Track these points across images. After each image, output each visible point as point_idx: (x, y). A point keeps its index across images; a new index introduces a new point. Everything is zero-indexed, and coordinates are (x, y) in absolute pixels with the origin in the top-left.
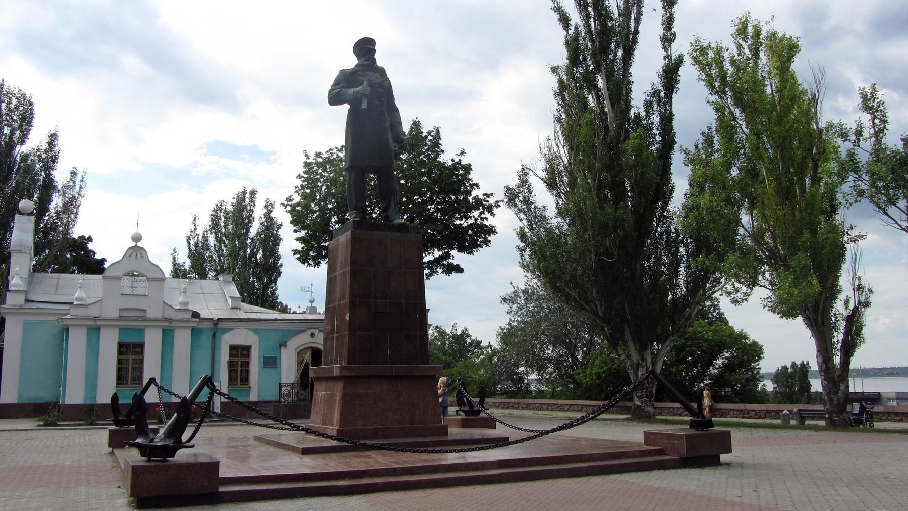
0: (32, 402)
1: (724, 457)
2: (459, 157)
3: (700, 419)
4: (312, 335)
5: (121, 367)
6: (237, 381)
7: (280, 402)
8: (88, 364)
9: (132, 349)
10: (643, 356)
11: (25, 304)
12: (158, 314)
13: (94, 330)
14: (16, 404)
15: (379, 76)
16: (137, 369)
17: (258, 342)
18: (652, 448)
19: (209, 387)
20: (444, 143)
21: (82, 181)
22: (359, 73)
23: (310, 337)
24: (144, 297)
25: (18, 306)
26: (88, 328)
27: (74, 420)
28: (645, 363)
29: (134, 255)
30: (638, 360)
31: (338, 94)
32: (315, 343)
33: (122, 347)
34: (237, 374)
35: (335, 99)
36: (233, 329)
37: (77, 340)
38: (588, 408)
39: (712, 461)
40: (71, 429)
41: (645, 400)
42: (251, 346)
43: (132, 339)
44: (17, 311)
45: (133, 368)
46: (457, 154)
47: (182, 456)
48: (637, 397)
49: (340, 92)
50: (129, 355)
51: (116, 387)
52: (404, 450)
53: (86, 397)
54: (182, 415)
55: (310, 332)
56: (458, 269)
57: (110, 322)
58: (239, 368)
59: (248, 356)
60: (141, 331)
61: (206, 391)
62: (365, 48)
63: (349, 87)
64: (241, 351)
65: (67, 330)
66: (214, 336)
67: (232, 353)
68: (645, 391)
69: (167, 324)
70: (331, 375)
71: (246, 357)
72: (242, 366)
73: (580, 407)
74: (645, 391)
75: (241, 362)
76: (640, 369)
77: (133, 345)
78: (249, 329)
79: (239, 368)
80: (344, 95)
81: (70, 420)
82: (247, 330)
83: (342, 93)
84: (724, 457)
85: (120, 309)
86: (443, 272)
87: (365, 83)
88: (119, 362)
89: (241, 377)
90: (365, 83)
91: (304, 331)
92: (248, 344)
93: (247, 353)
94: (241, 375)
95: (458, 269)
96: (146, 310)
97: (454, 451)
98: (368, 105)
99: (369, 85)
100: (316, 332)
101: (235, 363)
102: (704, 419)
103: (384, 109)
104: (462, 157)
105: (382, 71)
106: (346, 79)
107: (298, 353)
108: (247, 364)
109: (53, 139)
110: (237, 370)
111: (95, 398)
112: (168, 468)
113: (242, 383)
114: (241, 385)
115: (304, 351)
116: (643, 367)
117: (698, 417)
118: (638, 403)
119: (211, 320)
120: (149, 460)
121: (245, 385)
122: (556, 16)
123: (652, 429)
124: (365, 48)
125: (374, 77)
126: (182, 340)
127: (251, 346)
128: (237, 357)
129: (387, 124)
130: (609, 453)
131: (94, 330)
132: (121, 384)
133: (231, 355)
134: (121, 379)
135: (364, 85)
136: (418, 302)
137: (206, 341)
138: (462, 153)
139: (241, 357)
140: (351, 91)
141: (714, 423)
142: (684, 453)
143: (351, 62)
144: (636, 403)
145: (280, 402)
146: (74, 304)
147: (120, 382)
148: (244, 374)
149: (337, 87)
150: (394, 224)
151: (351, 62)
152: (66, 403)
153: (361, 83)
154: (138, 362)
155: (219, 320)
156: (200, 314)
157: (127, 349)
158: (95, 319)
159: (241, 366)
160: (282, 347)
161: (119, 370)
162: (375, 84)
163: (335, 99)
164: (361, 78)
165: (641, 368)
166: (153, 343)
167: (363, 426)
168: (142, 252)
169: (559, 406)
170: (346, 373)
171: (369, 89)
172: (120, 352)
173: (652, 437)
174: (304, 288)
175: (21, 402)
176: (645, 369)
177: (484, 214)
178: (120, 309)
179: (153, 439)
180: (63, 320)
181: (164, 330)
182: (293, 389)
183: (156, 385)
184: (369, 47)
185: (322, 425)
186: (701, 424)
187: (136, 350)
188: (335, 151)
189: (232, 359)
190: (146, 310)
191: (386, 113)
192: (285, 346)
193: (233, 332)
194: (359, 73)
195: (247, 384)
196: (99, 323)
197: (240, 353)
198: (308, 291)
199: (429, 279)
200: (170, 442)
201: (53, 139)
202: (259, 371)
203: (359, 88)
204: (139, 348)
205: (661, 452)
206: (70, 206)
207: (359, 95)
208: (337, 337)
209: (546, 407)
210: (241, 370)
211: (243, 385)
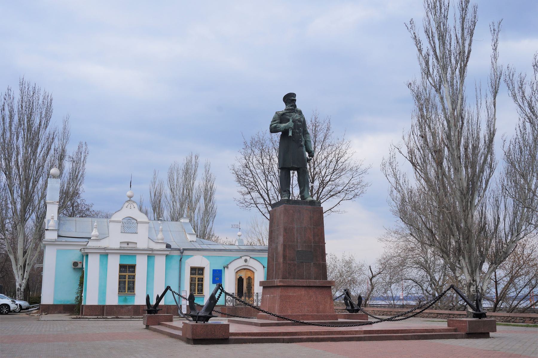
0: (62, 303)
1: (491, 334)
3: (478, 312)
4: (246, 261)
6: (195, 291)
7: (225, 306)
10: (473, 278)
11: (58, 238)
12: (145, 246)
14: (52, 305)
15: (298, 115)
16: (131, 282)
17: (209, 265)
18: (451, 328)
19: (220, 289)
22: (287, 114)
23: (244, 261)
25: (54, 239)
26: (100, 255)
27: (92, 315)
28: (475, 283)
29: (129, 206)
30: (470, 280)
31: (275, 127)
32: (247, 266)
34: (195, 287)
35: (273, 130)
36: (193, 256)
38: (441, 316)
39: (485, 335)
40: (102, 321)
42: (204, 267)
44: (52, 243)
47: (211, 321)
53: (99, 300)
54: (212, 302)
55: (244, 258)
58: (197, 283)
60: (134, 256)
62: (290, 99)
63: (281, 123)
64: (198, 271)
65: (87, 256)
66: (181, 260)
67: (121, 269)
69: (150, 252)
70: (273, 285)
71: (132, 273)
72: (198, 281)
73: (436, 314)
75: (198, 278)
76: (472, 287)
77: (134, 281)
78: (203, 256)
79: (197, 283)
81: (90, 315)
82: (202, 256)
83: (277, 126)
84: (491, 334)
85: (120, 242)
87: (291, 120)
88: (120, 277)
89: (198, 289)
90: (291, 120)
91: (241, 257)
92: (202, 266)
94: (198, 287)
96: (137, 243)
98: (292, 134)
99: (293, 121)
100: (248, 258)
101: (194, 279)
102: (480, 313)
103: (301, 134)
105: (300, 113)
106: (281, 118)
107: (236, 273)
108: (201, 280)
110: (195, 284)
111: (105, 301)
112: (207, 325)
113: (199, 293)
115: (240, 271)
116: (474, 286)
117: (477, 311)
119: (179, 250)
120: (197, 322)
121: (200, 294)
124: (290, 99)
125: (295, 116)
126: (160, 262)
127: (204, 267)
129: (303, 143)
130: (426, 329)
133: (191, 274)
136: (312, 227)
137: (175, 263)
139: (198, 275)
142: (468, 330)
143: (282, 107)
144: (469, 310)
145: (225, 306)
148: (200, 287)
150: (307, 201)
151: (282, 107)
152: (88, 304)
153: (288, 120)
154: (132, 277)
155: (184, 249)
156: (171, 246)
157: (125, 268)
158: (105, 249)
159: (198, 281)
160: (226, 268)
162: (296, 120)
164: (288, 117)
165: (473, 286)
166: (141, 263)
167: (291, 313)
171: (293, 124)
173: (451, 322)
174: (234, 225)
175: (55, 303)
176: (475, 287)
178: (120, 242)
179: (199, 313)
180: (85, 249)
182: (257, 297)
183: (171, 290)
184: (292, 98)
187: (131, 269)
190: (137, 243)
191: (302, 136)
192: (228, 268)
193: (193, 257)
194: (287, 114)
195: (133, 292)
196: (107, 251)
197: (197, 271)
198: (237, 228)
200: (207, 314)
202: (210, 285)
203: (287, 124)
204: (132, 268)
205: (455, 330)
207: (287, 128)
208: (276, 264)
211: (199, 294)
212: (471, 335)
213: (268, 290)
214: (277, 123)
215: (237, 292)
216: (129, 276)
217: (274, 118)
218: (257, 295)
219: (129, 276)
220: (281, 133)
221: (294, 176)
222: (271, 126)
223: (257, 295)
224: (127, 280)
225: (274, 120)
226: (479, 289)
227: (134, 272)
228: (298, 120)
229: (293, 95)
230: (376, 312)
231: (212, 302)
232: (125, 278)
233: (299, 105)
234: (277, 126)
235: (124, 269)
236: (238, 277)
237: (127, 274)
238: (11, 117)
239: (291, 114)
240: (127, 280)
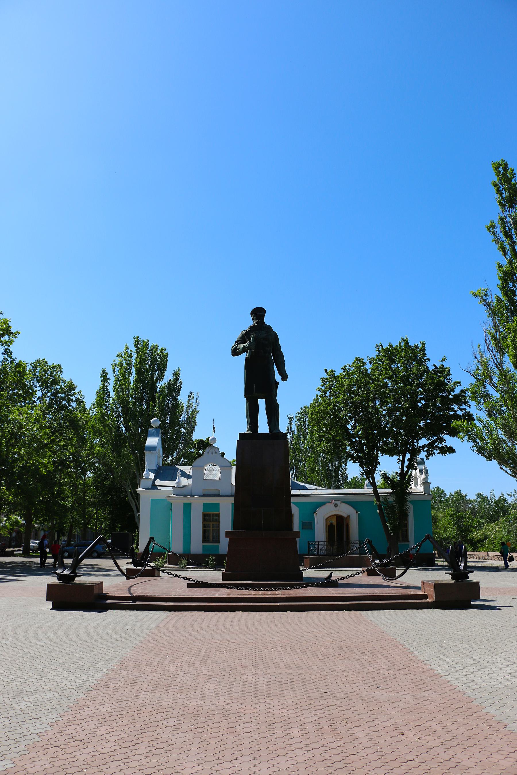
2: (441, 363)
5: (206, 530)
8: (185, 528)
9: (212, 517)
20: (429, 353)
21: (196, 402)
24: (427, 484)
33: (206, 516)
39: (467, 606)
46: (440, 361)
51: (202, 543)
52: (260, 590)
56: (451, 450)
61: (152, 544)
80: (239, 349)
86: (439, 453)
88: (204, 526)
95: (451, 450)
97: (270, 590)
100: (339, 503)
104: (444, 363)
107: (326, 519)
109: (177, 374)
115: (331, 517)
122: (496, 247)
134: (206, 538)
138: (444, 360)
146: (175, 487)
147: (205, 540)
151: (249, 322)
161: (204, 532)
163: (235, 352)
168: (216, 450)
172: (204, 520)
177: (462, 406)
182: (319, 546)
188: (348, 367)
189: (205, 523)
199: (429, 459)
201: (177, 374)
206: (191, 422)
210: (212, 529)
215: (328, 540)
218: (319, 544)
221: (262, 403)
222: (232, 348)
223: (319, 544)
233: (268, 320)
236: (329, 523)
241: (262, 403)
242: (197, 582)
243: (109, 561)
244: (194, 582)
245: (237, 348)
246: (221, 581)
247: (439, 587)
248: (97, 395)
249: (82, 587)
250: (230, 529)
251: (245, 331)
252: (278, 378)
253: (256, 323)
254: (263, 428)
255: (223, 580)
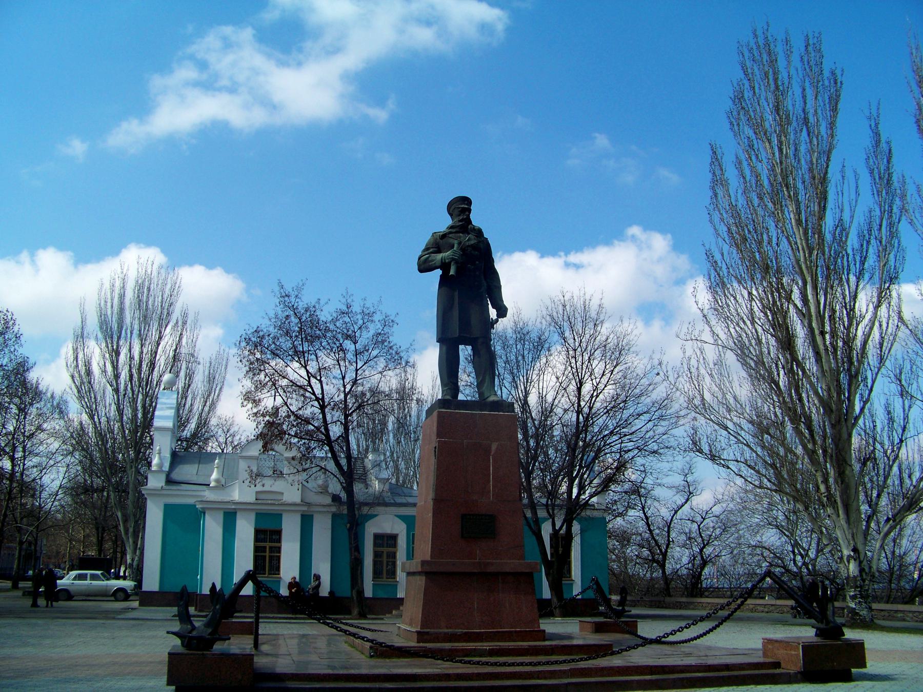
13: (230, 517)
22: (450, 235)
31: (426, 261)
34: (382, 567)
35: (424, 267)
37: (213, 528)
39: (845, 677)
41: (860, 602)
42: (397, 535)
43: (269, 525)
44: (156, 493)
45: (271, 558)
47: (218, 647)
48: (850, 596)
49: (428, 258)
50: (267, 542)
57: (244, 507)
59: (395, 545)
60: (278, 517)
64: (387, 540)
68: (859, 589)
69: (305, 508)
74: (859, 589)
75: (387, 553)
77: (270, 531)
80: (433, 261)
88: (257, 549)
92: (395, 532)
93: (393, 542)
94: (387, 567)
105: (479, 233)
106: (438, 244)
108: (394, 556)
114: (387, 578)
117: (822, 623)
118: (853, 605)
123: (785, 635)
127: (397, 535)
128: (383, 547)
131: (230, 517)
132: (377, 578)
133: (375, 545)
135: (455, 249)
140: (439, 256)
141: (72, 593)
149: (426, 252)
151: (444, 222)
163: (424, 267)
164: (451, 241)
169: (778, 607)
170: (428, 569)
172: (257, 540)
181: (302, 516)
185: (447, 628)
186: (830, 632)
190: (283, 493)
209: (761, 609)
211: (389, 578)
212: (810, 675)
213: (410, 578)
214: (432, 253)
216: (271, 548)
217: (427, 245)
219: (271, 548)
220: (439, 272)
221: (465, 351)
222: (419, 259)
224: (267, 554)
225: (427, 249)
226: (864, 566)
227: (279, 541)
228: (472, 246)
229: (466, 201)
230: (704, 605)
231: (217, 607)
232: (265, 552)
233: (476, 219)
234: (430, 259)
235: (263, 536)
237: (268, 545)
238: (112, 299)
239: (458, 235)
240: (267, 554)
241: (465, 351)
242: (385, 646)
243: (858, 685)
244: (373, 643)
245: (430, 259)
246: (413, 643)
247: (808, 649)
248: (433, 235)
249: (226, 656)
250: (428, 558)
251: (441, 234)
252: (493, 313)
253: (460, 221)
254: (467, 391)
255: (418, 642)
